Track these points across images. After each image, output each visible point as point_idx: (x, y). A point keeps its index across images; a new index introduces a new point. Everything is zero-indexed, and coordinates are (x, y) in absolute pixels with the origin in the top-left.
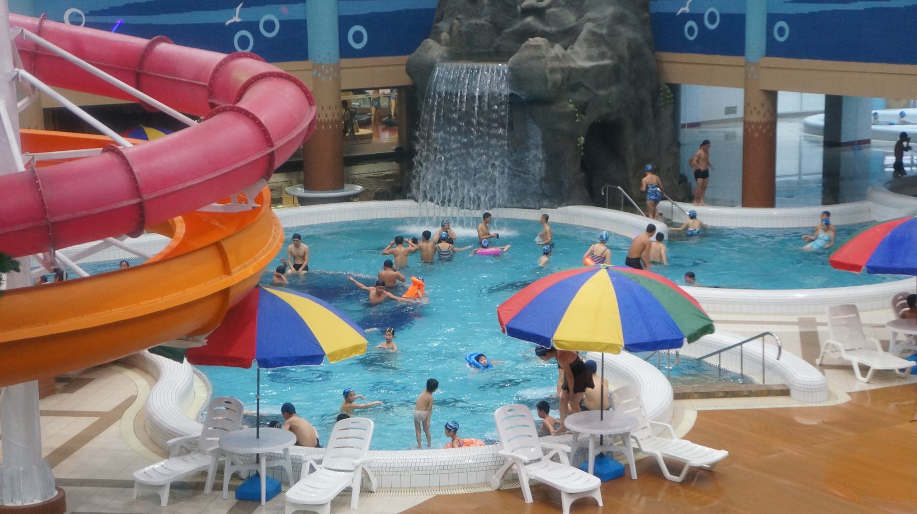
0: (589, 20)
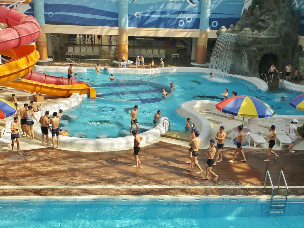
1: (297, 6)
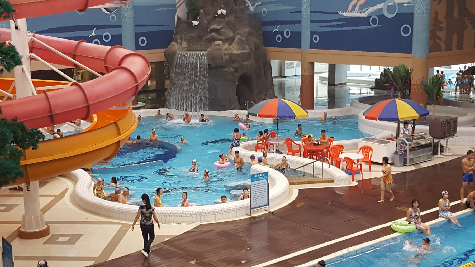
0: (238, 34)
1: (252, 8)
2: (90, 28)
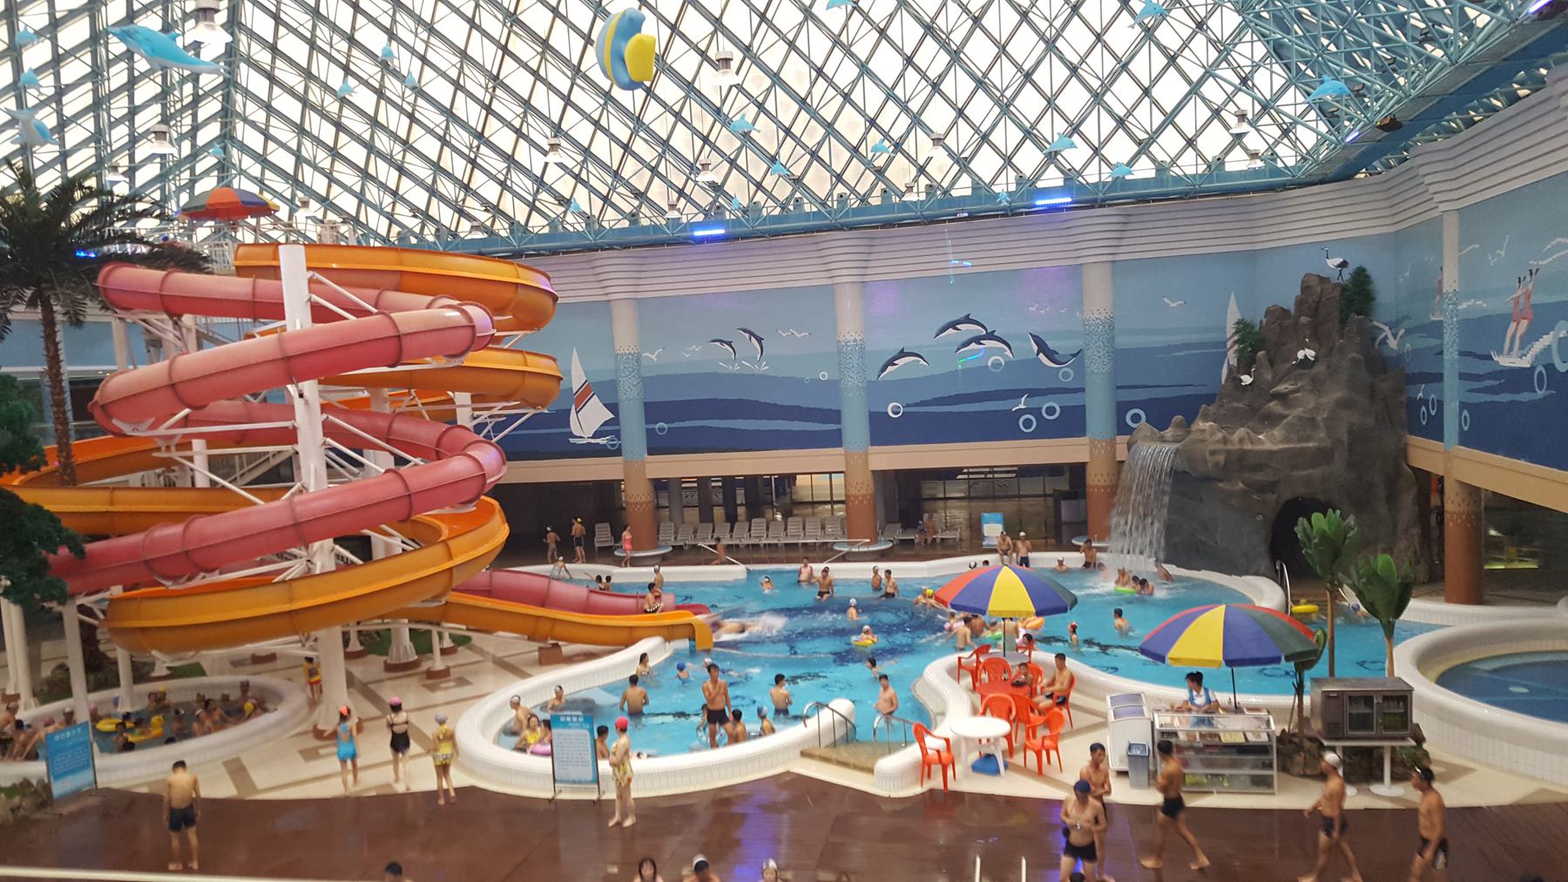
2: (1016, 394)
